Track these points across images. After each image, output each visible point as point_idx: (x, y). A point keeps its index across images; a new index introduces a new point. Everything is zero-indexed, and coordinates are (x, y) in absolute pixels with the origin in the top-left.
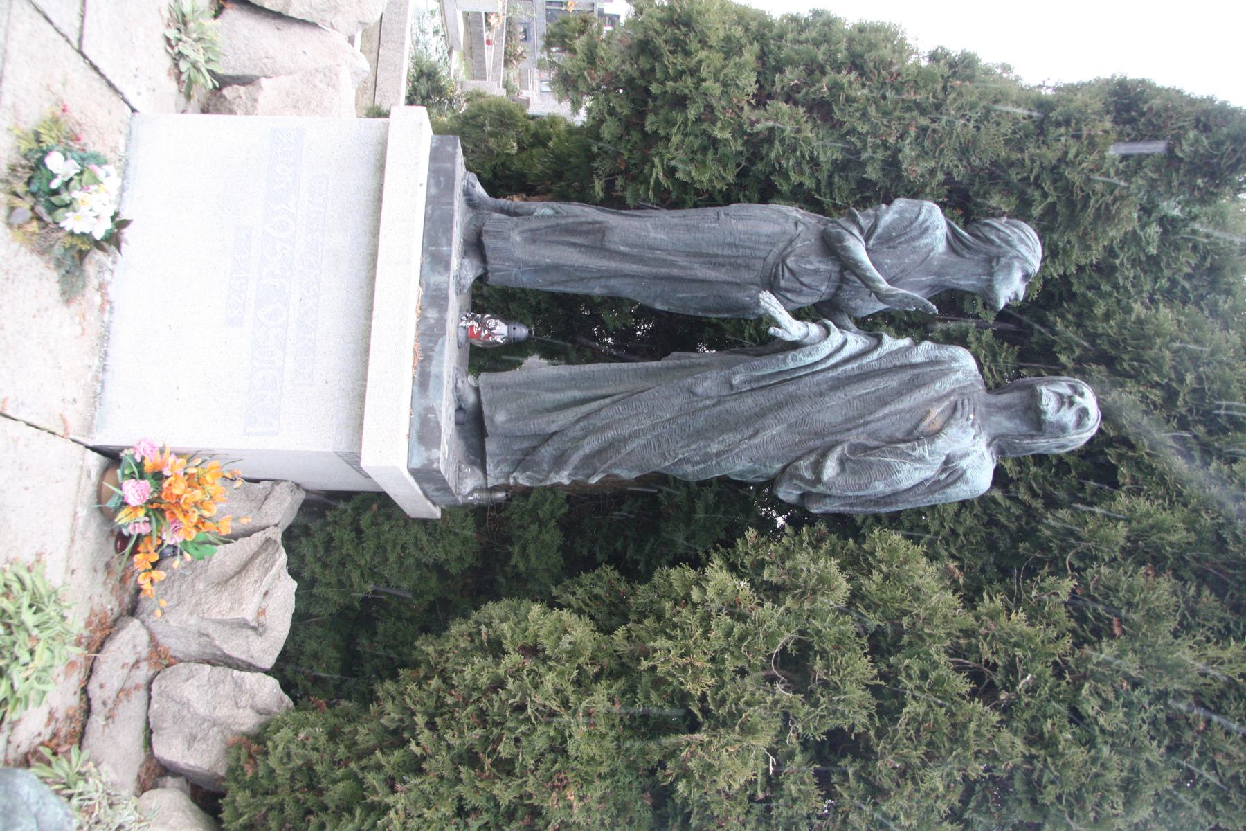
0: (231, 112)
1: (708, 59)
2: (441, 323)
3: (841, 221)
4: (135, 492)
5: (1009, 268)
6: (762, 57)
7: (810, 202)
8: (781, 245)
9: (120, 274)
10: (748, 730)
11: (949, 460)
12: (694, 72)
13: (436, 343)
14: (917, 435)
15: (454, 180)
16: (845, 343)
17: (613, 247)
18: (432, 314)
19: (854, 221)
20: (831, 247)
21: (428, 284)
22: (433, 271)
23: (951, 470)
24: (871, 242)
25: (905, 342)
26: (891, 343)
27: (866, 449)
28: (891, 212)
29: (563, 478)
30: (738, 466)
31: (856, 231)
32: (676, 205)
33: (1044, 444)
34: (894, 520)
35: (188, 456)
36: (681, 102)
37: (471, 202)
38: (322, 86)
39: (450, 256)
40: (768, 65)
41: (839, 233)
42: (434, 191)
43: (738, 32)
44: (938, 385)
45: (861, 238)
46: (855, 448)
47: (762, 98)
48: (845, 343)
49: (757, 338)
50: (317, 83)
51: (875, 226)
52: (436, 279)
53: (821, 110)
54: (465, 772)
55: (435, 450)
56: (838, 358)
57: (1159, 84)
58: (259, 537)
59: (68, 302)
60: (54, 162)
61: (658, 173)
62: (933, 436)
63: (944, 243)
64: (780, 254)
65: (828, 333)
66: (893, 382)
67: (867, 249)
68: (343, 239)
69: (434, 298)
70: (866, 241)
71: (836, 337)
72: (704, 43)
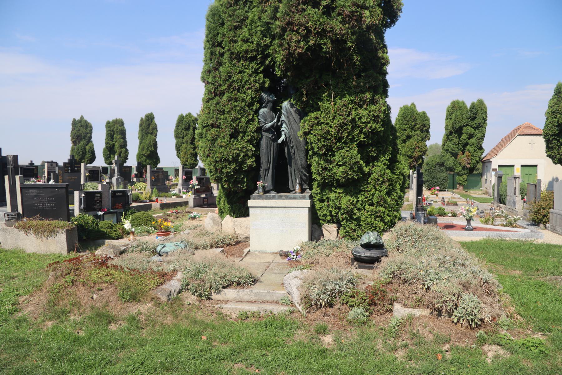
2: (285, 196)
18: (283, 198)
19: (263, 126)
25: (282, 115)
26: (283, 118)
69: (280, 198)
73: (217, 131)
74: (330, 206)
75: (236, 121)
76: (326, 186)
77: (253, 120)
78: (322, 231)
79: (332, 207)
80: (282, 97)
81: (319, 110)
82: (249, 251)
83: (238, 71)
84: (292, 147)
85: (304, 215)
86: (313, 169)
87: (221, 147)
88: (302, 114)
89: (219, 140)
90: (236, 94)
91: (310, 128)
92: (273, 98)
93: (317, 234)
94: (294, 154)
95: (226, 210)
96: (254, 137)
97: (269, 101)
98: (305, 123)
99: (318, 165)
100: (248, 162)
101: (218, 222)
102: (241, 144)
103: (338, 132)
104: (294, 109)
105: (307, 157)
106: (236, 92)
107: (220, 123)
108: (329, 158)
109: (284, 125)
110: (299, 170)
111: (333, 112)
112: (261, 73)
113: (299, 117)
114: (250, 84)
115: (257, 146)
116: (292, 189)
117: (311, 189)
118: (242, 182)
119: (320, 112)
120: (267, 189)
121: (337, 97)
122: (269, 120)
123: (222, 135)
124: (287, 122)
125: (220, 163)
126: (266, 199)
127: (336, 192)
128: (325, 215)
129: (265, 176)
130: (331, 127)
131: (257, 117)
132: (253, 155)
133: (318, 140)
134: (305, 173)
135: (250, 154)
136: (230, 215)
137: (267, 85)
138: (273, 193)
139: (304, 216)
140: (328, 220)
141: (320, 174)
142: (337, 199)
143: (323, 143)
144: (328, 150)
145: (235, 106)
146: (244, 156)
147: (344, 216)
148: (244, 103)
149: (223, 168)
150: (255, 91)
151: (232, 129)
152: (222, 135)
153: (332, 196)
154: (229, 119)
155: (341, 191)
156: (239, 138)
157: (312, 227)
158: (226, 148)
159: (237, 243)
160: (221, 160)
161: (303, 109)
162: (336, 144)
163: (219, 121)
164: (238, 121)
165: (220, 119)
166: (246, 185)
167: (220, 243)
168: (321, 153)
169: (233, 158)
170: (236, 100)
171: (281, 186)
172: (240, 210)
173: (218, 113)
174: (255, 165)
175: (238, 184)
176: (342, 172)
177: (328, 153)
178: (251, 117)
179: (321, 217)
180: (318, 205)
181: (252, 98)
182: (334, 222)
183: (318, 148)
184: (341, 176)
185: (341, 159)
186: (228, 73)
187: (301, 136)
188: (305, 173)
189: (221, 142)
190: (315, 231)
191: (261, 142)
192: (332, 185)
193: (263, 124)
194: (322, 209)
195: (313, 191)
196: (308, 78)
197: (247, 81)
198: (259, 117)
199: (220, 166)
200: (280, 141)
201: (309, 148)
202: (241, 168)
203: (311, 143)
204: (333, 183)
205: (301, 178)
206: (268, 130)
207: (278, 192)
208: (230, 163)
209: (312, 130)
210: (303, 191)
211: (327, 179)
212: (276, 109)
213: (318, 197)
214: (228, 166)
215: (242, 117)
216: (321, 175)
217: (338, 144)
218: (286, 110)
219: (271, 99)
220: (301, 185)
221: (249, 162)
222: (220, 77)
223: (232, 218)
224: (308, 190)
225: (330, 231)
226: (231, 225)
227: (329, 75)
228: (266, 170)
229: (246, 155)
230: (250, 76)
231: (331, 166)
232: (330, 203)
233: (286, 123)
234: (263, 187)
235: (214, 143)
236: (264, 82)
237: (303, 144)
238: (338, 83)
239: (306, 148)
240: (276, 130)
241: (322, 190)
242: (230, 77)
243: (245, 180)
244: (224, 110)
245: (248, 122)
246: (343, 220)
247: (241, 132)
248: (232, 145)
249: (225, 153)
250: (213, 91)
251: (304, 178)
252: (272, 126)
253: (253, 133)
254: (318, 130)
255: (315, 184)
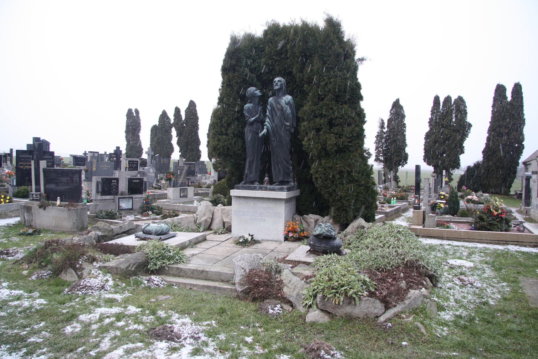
1: (221, 144)
2: (264, 187)
4: (291, 235)
5: (255, 94)
6: (220, 135)
7: (243, 127)
9: (256, 238)
10: (326, 138)
11: (286, 104)
12: (223, 146)
14: (282, 109)
20: (252, 124)
23: (288, 103)
26: (268, 113)
27: (285, 118)
29: (291, 168)
30: (288, 139)
32: (245, 148)
33: (284, 88)
34: (297, 113)
35: (286, 226)
36: (228, 149)
37: (245, 183)
40: (221, 134)
43: (216, 139)
46: (284, 120)
47: (227, 134)
49: (266, 137)
52: (258, 188)
53: (229, 125)
54: (335, 183)
57: (222, 64)
58: (302, 220)
60: (241, 241)
61: (240, 152)
62: (282, 107)
68: (251, 203)
71: (266, 123)
72: (218, 145)
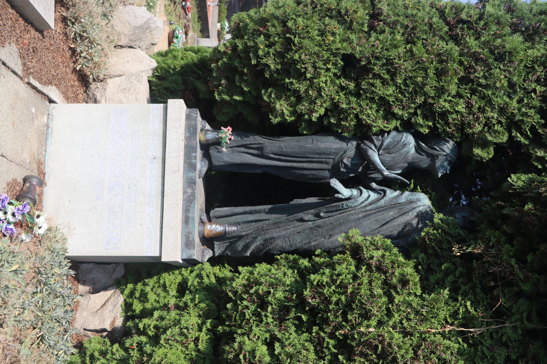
0: (95, 101)
2: (193, 195)
3: (366, 142)
8: (341, 153)
13: (191, 203)
15: (196, 129)
16: (369, 196)
17: (267, 155)
18: (189, 191)
19: (372, 142)
21: (187, 177)
22: (189, 171)
24: (381, 152)
25: (398, 192)
26: (391, 194)
28: (389, 138)
31: (373, 147)
38: (135, 82)
39: (196, 164)
41: (366, 149)
42: (188, 135)
44: (411, 213)
45: (376, 150)
48: (369, 196)
50: (133, 80)
51: (382, 144)
55: (192, 250)
56: (366, 203)
59: (100, 350)
63: (414, 149)
64: (341, 157)
65: (361, 194)
66: (392, 213)
67: (379, 155)
69: (190, 183)
70: (378, 151)
73: (362, 25)
74: (165, 313)
75: (388, 71)
76: (218, 302)
77: (389, 115)
78: (105, 289)
79: (162, 318)
80: (441, 190)
81: (423, 289)
82: (51, 101)
83: (515, 79)
84: (317, 216)
85: (142, 247)
86: (262, 268)
87: (322, 33)
88: (407, 242)
89: (339, 30)
90: (456, 73)
91: (373, 262)
92: (442, 168)
93: (99, 275)
94: (302, 220)
95: (169, 61)
96: (346, 119)
97: (433, 158)
98: (386, 249)
99: (271, 285)
100: (282, 102)
101: (140, 40)
102: (329, 86)
103: (368, 344)
104: (415, 222)
105: (292, 253)
106: (462, 74)
107: (383, 32)
108: (292, 315)
109: (374, 196)
110: (259, 231)
111: (422, 329)
112: (511, 138)
113: (395, 233)
114: (481, 110)
115: (322, 128)
116: (212, 213)
117: (213, 261)
118: (232, 89)
119: (419, 292)
120: (213, 152)
121: (465, 340)
122: (388, 158)
123: (353, 37)
124: (382, 202)
125: (279, 29)
126: (186, 147)
127: (200, 330)
128: (144, 297)
129: (245, 146)
130: (380, 323)
131: (396, 129)
132: (299, 116)
133: (343, 286)
134: (253, 247)
135: (303, 107)
136: (156, 69)
137: (477, 151)
138: (201, 166)
139: (136, 243)
140: (131, 305)
141: (247, 287)
142: (182, 334)
143: (334, 299)
144: (313, 312)
145: (425, 70)
146: (296, 93)
147: (135, 354)
148: (432, 93)
149: (267, 36)
150: (463, 123)
151: (369, 63)
152: (353, 37)
153: (192, 319)
154: (393, 53)
155: (202, 346)
156: (343, 82)
157: (117, 264)
158: (320, 46)
159: (83, 79)
160: (289, 30)
161: (422, 246)
162: (332, 336)
163: (387, 29)
164: (386, 76)
165: (392, 33)
166: (223, 100)
167: (77, 28)
168: (307, 293)
169: (294, 62)
170: (440, 74)
171: (224, 187)
172: (162, 88)
173: (407, 27)
174: (275, 120)
175: (227, 78)
176: (253, 352)
177: (304, 312)
178: (396, 110)
179: (139, 286)
180: (172, 279)
181: (444, 115)
182: (127, 319)
183: (320, 285)
184: (241, 348)
185: (289, 350)
186: (510, 53)
187: (348, 238)
188: (253, 247)
189: (333, 34)
190: (91, 272)
191: (332, 139)
192: (219, 320)
193: (378, 143)
194: (159, 291)
195: (207, 266)
196: (521, 261)
197: (490, 102)
198: (393, 133)
199: (272, 30)
200: (336, 183)
201: (317, 259)
202: (267, 84)
203: (332, 266)
204: (223, 324)
205: (240, 237)
206: (361, 155)
207: (208, 179)
208: (280, 55)
209: (369, 268)
210: (208, 241)
211: (236, 305)
212: (415, 176)
213: (193, 281)
214: (272, 51)
215: (397, 87)
216: (247, 292)
217: (332, 342)
218: (411, 202)
219: (438, 163)
220: (221, 237)
221: (282, 106)
222: (496, 36)
223: (150, 73)
224: (209, 254)
225: (103, 310)
226: (134, 68)
227: (529, 319)
228: (261, 149)
229: (299, 99)
230: (502, 110)
231: (270, 320)
232: (173, 314)
233: (378, 200)
234: (218, 143)
235: (331, 17)
236: (484, 145)
237: (328, 243)
238: (505, 345)
239: (318, 252)
240: (360, 175)
241: (208, 289)
242: (500, 58)
243: (236, 98)
244: (414, 43)
245: (384, 105)
246: (126, 350)
247: (358, 86)
248: (326, 62)
249: (306, 42)
250: (464, 16)
251: (240, 245)
252: (371, 166)
253: (357, 116)
254: (370, 287)
255: (226, 272)
